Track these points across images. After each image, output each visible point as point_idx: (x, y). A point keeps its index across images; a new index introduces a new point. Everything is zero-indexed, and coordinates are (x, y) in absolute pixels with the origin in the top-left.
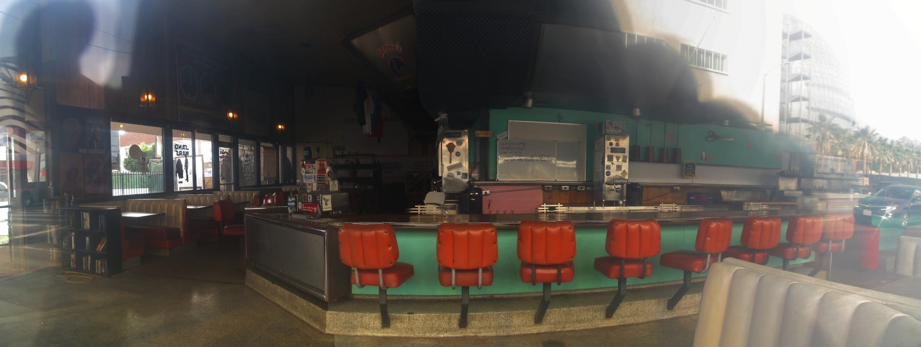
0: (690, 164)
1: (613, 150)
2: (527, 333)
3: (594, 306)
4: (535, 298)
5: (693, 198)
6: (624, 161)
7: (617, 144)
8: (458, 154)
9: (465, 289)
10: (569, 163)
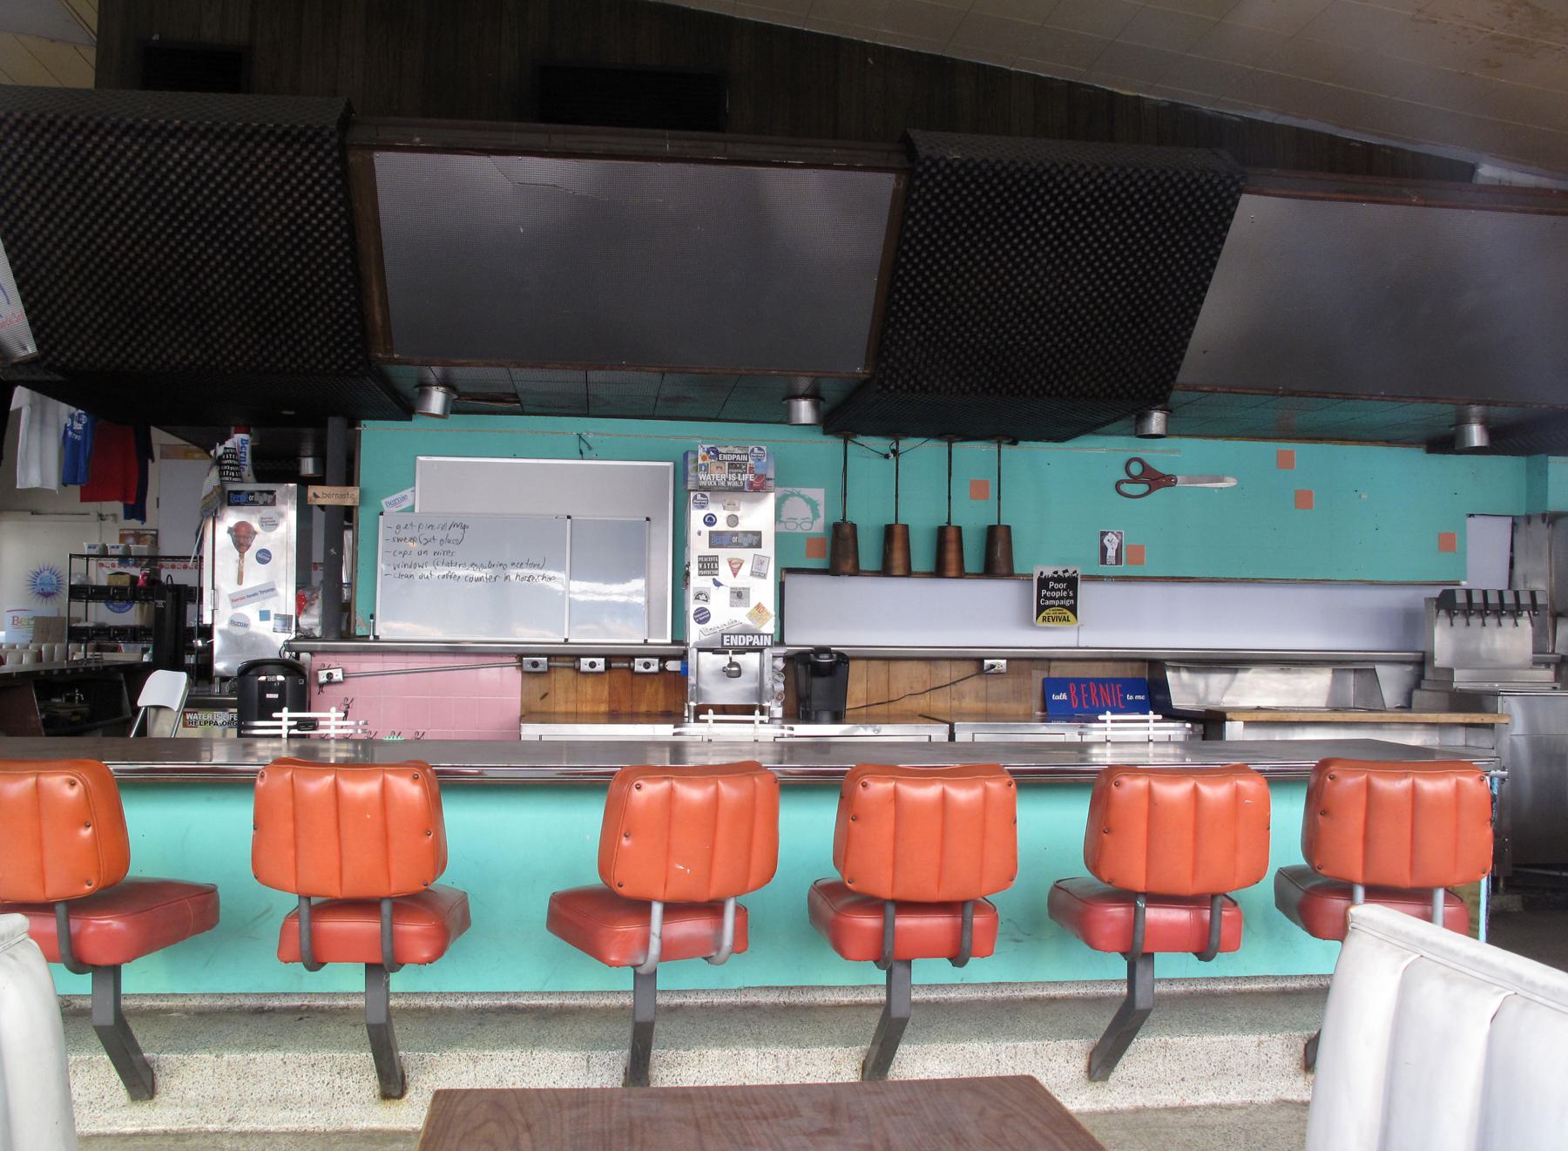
0: (1059, 580)
1: (717, 540)
2: (101, 1130)
3: (337, 1055)
4: (606, 1014)
5: (1063, 696)
6: (758, 574)
7: (733, 520)
8: (264, 557)
9: (377, 971)
10: (616, 588)
